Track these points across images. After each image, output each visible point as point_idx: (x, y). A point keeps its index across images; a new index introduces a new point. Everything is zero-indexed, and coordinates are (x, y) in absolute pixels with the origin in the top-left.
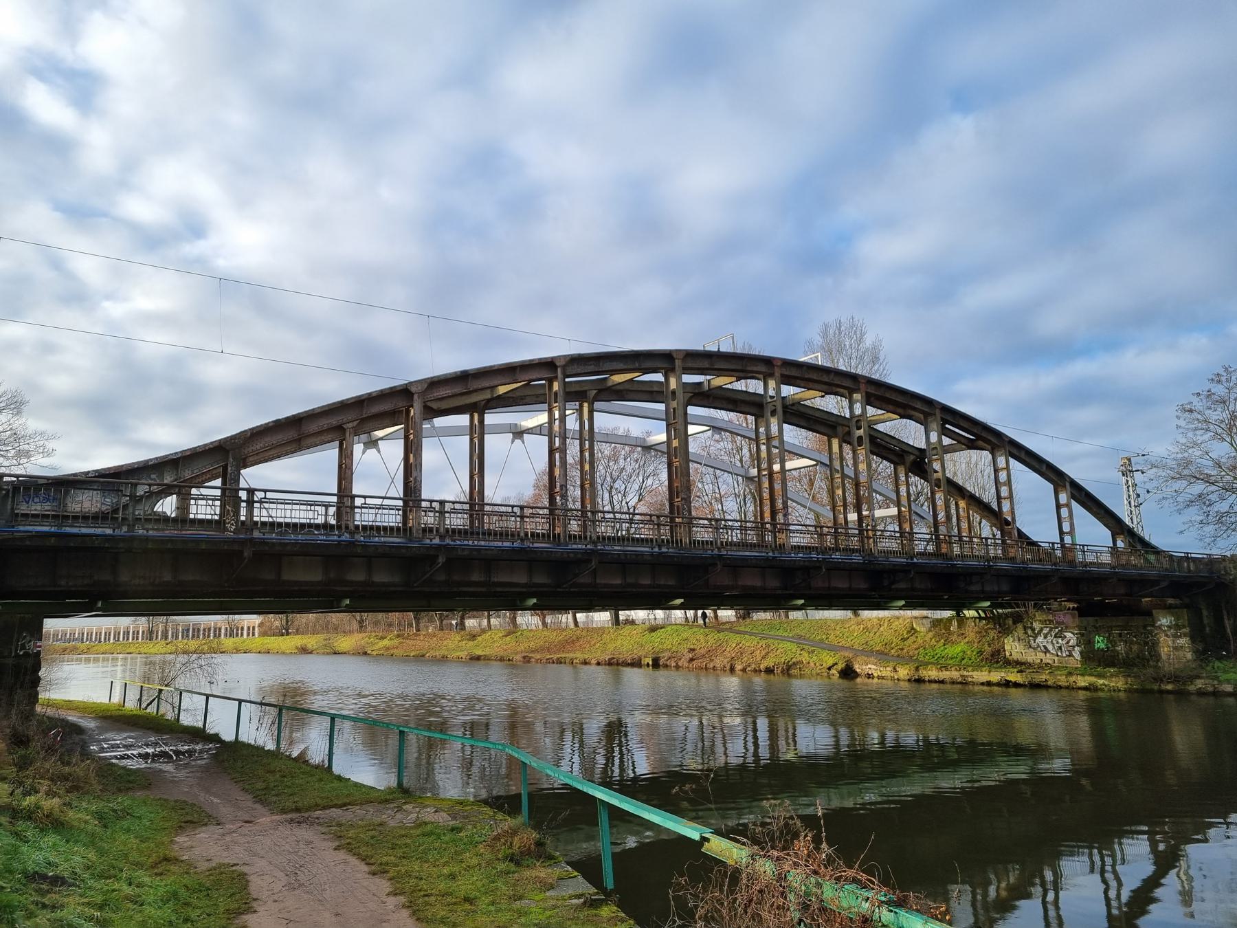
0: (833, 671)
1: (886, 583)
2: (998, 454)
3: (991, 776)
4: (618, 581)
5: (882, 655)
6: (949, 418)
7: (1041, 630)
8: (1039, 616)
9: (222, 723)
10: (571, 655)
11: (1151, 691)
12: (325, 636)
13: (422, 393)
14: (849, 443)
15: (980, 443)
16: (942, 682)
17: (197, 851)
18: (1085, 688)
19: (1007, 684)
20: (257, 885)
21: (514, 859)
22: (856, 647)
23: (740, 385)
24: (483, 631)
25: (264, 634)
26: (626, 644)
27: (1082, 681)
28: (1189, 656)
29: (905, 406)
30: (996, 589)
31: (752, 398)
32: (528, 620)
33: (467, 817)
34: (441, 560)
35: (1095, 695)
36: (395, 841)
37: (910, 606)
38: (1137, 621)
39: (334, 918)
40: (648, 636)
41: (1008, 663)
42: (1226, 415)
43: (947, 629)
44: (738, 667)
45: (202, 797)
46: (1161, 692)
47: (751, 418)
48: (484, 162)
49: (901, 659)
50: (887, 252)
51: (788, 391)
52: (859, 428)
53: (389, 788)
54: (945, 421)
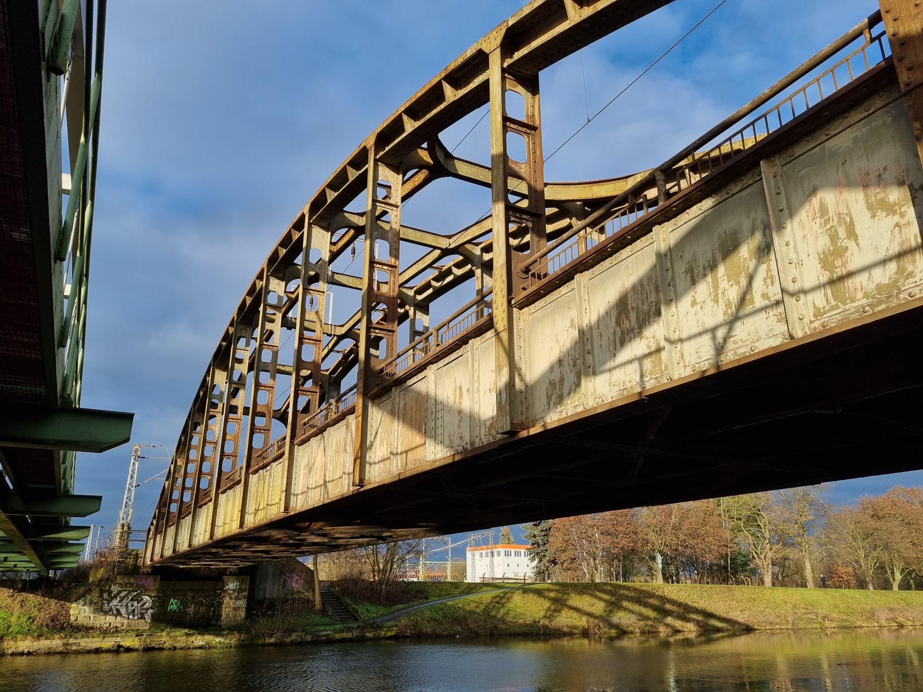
7: (120, 592)
18: (201, 648)
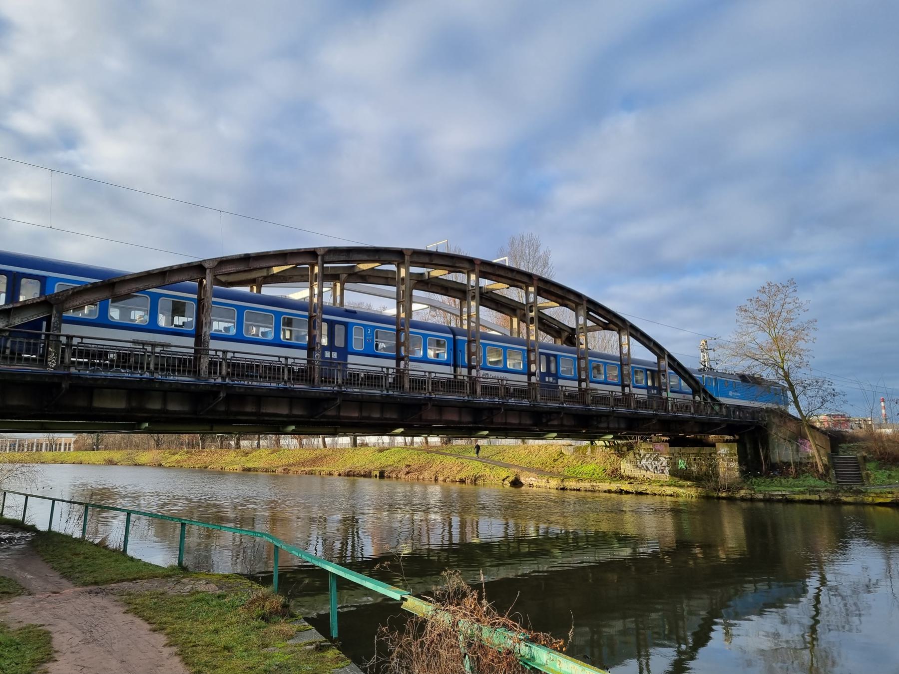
0: (506, 482)
1: (544, 421)
2: (622, 334)
3: (604, 555)
4: (356, 415)
5: (540, 472)
6: (593, 307)
8: (644, 445)
9: (38, 518)
10: (319, 469)
11: (713, 498)
12: (128, 451)
13: (213, 269)
14: (524, 322)
15: (611, 326)
16: (579, 490)
17: (11, 615)
18: (671, 495)
19: (621, 492)
20: (59, 641)
21: (265, 618)
22: (522, 465)
23: (452, 277)
24: (254, 450)
25: (78, 449)
26: (361, 460)
27: (669, 490)
28: (737, 474)
29: (563, 298)
30: (617, 426)
31: (459, 287)
32: (289, 442)
33: (231, 587)
34: (222, 395)
35: (677, 499)
36: (173, 606)
37: (560, 437)
38: (707, 450)
39: (119, 665)
40: (377, 455)
41: (622, 477)
42: (767, 315)
43: (584, 454)
44: (441, 479)
45: (18, 574)
46: (719, 498)
47: (458, 301)
48: (299, 112)
49: (552, 474)
50: (572, 197)
51: (485, 283)
52: (531, 311)
53: (171, 566)
54: (589, 310)
